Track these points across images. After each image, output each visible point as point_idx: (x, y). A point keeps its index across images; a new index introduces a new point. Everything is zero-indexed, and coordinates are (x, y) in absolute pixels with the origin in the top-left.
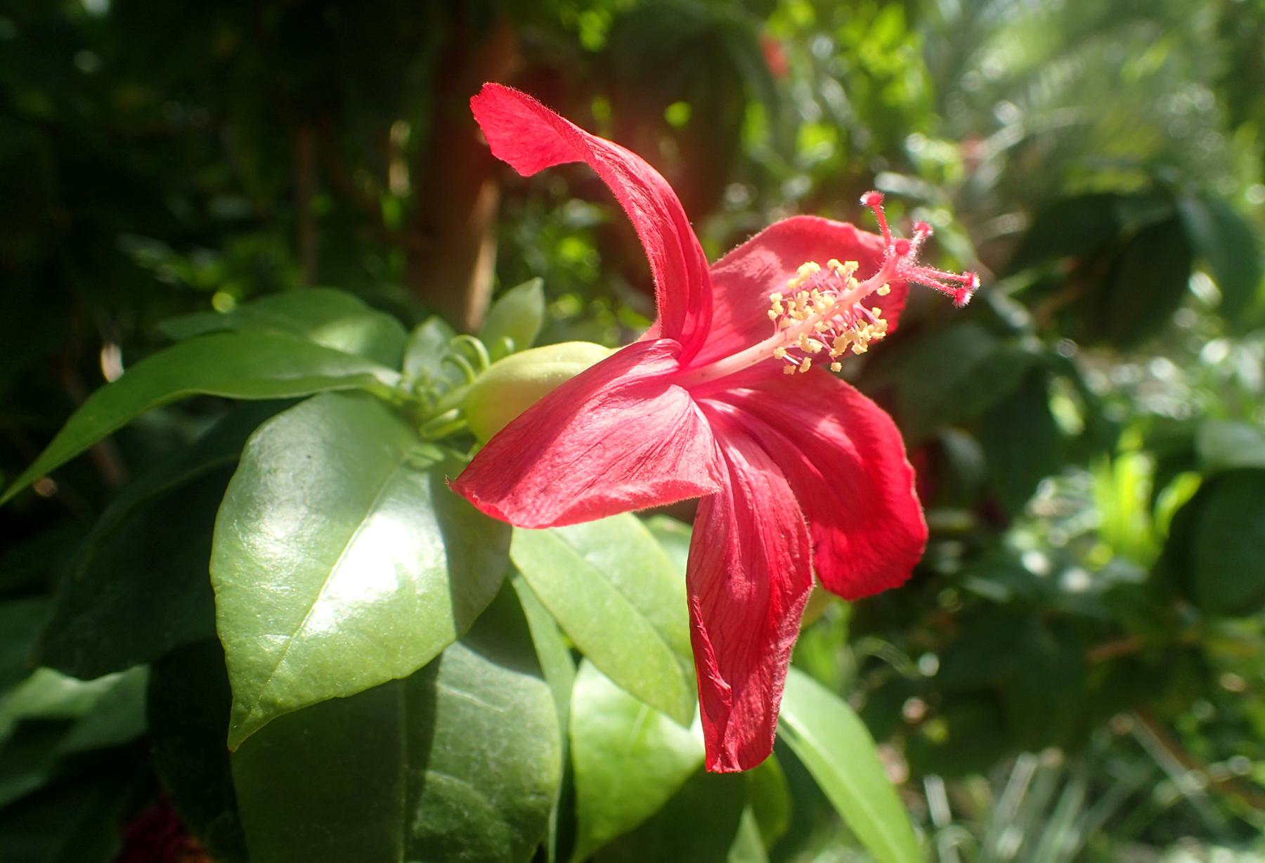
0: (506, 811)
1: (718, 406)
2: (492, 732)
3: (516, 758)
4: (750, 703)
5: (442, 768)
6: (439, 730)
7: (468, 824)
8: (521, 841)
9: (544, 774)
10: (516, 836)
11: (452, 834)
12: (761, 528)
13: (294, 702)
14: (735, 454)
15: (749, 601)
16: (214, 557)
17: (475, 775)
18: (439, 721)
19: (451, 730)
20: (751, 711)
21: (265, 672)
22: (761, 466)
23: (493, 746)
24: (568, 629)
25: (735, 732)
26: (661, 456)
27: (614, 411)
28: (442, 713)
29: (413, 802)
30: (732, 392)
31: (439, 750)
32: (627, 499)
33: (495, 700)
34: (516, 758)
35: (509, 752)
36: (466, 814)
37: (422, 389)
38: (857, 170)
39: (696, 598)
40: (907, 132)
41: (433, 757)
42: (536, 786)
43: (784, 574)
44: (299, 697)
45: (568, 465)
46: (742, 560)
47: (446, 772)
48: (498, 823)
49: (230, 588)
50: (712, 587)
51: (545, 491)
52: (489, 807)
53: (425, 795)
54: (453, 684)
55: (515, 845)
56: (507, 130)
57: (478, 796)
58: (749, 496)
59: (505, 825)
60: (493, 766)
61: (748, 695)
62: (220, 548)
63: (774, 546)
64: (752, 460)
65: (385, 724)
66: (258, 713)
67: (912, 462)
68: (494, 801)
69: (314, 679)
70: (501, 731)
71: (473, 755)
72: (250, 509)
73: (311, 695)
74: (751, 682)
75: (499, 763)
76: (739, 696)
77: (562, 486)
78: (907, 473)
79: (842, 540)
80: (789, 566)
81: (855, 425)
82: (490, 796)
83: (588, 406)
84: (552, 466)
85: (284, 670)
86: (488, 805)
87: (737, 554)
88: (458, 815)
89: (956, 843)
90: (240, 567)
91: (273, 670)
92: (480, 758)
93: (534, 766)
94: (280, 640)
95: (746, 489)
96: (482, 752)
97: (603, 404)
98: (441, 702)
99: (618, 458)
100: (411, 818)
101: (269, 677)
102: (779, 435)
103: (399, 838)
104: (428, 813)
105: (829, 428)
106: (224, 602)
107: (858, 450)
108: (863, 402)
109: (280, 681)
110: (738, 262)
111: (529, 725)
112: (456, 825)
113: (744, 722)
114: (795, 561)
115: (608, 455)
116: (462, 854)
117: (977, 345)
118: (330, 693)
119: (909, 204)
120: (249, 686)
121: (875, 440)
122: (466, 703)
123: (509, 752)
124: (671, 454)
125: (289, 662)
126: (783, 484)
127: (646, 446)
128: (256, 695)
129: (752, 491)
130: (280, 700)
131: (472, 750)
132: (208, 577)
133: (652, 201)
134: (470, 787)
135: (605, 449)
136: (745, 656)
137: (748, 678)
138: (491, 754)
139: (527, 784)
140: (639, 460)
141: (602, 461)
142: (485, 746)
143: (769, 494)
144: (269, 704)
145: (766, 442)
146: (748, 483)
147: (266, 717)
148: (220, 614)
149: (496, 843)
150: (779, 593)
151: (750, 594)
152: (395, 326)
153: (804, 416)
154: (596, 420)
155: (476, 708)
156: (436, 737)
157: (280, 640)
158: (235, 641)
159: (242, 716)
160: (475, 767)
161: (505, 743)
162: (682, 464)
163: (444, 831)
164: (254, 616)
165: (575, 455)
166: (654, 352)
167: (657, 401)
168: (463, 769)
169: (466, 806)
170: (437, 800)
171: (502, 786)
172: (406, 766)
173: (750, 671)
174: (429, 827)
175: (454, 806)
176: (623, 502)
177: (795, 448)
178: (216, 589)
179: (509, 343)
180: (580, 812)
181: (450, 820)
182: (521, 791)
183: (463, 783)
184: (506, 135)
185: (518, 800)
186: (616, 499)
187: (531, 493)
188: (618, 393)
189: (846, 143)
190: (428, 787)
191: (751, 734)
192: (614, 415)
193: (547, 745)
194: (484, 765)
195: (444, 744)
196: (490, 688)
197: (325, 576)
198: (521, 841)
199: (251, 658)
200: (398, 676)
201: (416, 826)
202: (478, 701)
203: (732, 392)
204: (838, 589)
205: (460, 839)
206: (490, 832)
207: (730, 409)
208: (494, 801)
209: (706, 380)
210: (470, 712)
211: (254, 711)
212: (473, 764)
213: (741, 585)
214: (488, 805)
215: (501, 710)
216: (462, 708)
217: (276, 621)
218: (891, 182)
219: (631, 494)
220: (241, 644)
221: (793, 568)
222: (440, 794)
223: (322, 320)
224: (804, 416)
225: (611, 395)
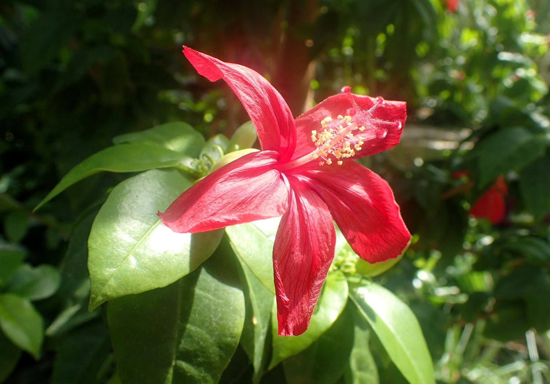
0: (218, 343)
1: (301, 178)
2: (216, 310)
3: (224, 322)
4: (302, 307)
5: (194, 324)
6: (194, 308)
7: (202, 347)
8: (224, 356)
9: (236, 329)
10: (222, 354)
11: (195, 351)
12: (309, 232)
13: (114, 295)
14: (304, 201)
15: (302, 264)
16: (90, 237)
17: (207, 327)
18: (194, 304)
19: (199, 308)
20: (302, 310)
21: (104, 283)
22: (316, 205)
23: (215, 316)
24: (253, 269)
25: (293, 319)
26: (250, 202)
27: (232, 183)
28: (196, 301)
29: (181, 336)
30: (310, 171)
31: (194, 316)
32: (224, 221)
33: (219, 298)
34: (224, 322)
35: (221, 319)
36: (201, 343)
37: (200, 167)
38: (489, 50)
39: (276, 261)
40: (520, 33)
41: (191, 319)
42: (231, 334)
43: (323, 252)
44: (117, 293)
45: (205, 206)
46: (300, 246)
47: (195, 325)
48: (215, 348)
49: (94, 249)
50: (284, 257)
51: (193, 217)
52: (211, 341)
53: (185, 334)
54: (201, 289)
55: (221, 357)
56: (200, 63)
57: (208, 336)
58: (306, 218)
59: (217, 349)
60: (214, 324)
61: (302, 304)
62: (93, 233)
63: (318, 239)
64: (312, 202)
65: (171, 303)
66: (100, 298)
67: (398, 203)
68: (213, 338)
69: (123, 286)
70: (219, 310)
71: (207, 319)
72: (114, 215)
73: (122, 292)
74: (304, 298)
75: (217, 323)
76: (297, 304)
77: (201, 215)
78: (397, 208)
79: (365, 238)
80: (326, 248)
81: (370, 187)
82: (212, 337)
83: (221, 180)
84: (198, 207)
85: (112, 282)
86: (211, 340)
87: (298, 243)
88: (198, 343)
89: (540, 369)
90: (100, 241)
91: (107, 282)
92: (209, 321)
93: (232, 325)
94: (113, 270)
95: (305, 215)
96: (210, 318)
97: (226, 180)
98: (196, 297)
99: (229, 203)
100: (180, 343)
101: (105, 284)
102: (328, 191)
103: (174, 350)
104: (186, 341)
105: (357, 189)
106: (92, 254)
107: (370, 197)
108: (375, 175)
109: (110, 286)
110: (310, 115)
111: (232, 308)
112: (197, 347)
113: (299, 315)
114: (329, 246)
115: (225, 201)
116: (199, 359)
117: (523, 137)
118: (130, 292)
119: (514, 66)
120: (97, 287)
121: (382, 193)
122: (206, 298)
123: (221, 319)
124: (256, 201)
125: (114, 279)
126: (327, 214)
127: (244, 198)
128: (100, 291)
129: (308, 216)
130: (109, 294)
131: (206, 317)
132: (87, 244)
133: (256, 92)
134: (204, 332)
135: (223, 199)
136: (301, 286)
137: (302, 296)
138: (214, 319)
139: (227, 332)
140: (239, 204)
141: (220, 205)
142: (212, 316)
143: (318, 217)
144: (105, 295)
145: (322, 194)
146: (307, 212)
147: (103, 300)
148: (89, 259)
149: (213, 356)
150: (320, 260)
151: (302, 260)
152: (202, 138)
153: (342, 182)
154: (224, 187)
155: (210, 300)
156: (192, 311)
157: (113, 270)
158: (94, 270)
159: (94, 299)
160: (207, 324)
161: (220, 315)
162: (262, 207)
163: (192, 349)
164: (102, 260)
165: (208, 202)
166: (259, 156)
167: (256, 178)
168: (201, 325)
169: (202, 340)
170: (190, 336)
171: (217, 333)
172: (179, 322)
173: (304, 293)
174: (186, 347)
175: (197, 339)
176: (223, 223)
177: (337, 197)
178: (89, 249)
179: (237, 147)
180: (274, 345)
181: (195, 345)
182: (225, 336)
183: (201, 330)
184: (201, 65)
185: (224, 339)
186: (218, 222)
187: (187, 218)
188: (235, 175)
189: (484, 37)
190: (187, 331)
191: (301, 320)
192: (231, 185)
193: (238, 317)
194: (211, 323)
195: (195, 314)
196: (217, 292)
197: (137, 246)
198: (224, 356)
199: (99, 277)
200: (161, 286)
201: (181, 346)
202: (210, 297)
203: (310, 171)
204: (368, 258)
205: (198, 353)
206: (211, 351)
207: (307, 179)
208: (213, 338)
209: (294, 167)
210: (207, 301)
211: (98, 297)
212: (206, 323)
213: (298, 256)
214: (211, 340)
215: (220, 301)
216: (204, 300)
217: (111, 263)
218: (505, 56)
219: (226, 220)
220: (95, 271)
221: (328, 250)
222: (192, 334)
223: (171, 137)
224: (342, 182)
225: (230, 176)
